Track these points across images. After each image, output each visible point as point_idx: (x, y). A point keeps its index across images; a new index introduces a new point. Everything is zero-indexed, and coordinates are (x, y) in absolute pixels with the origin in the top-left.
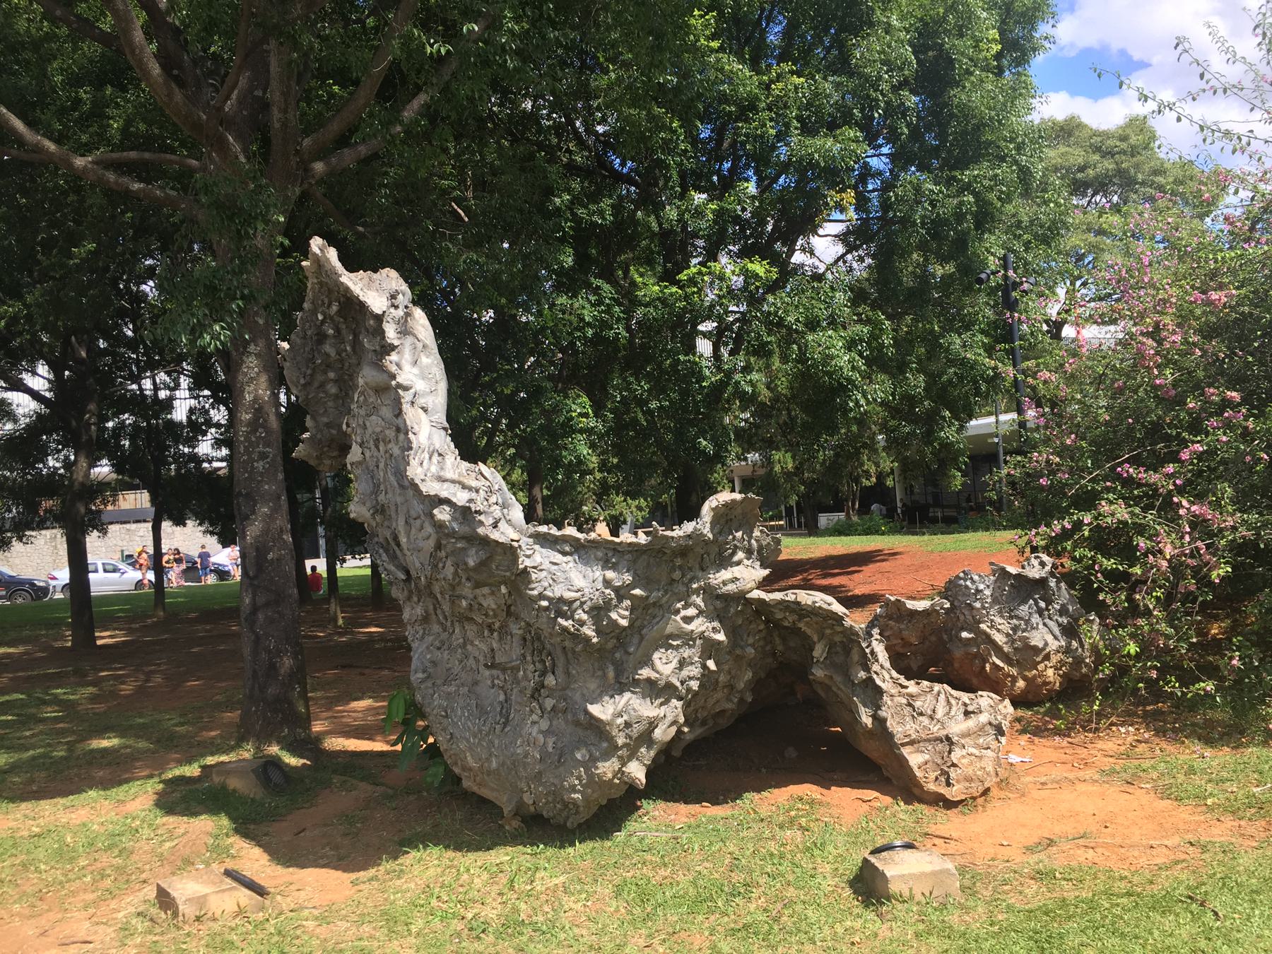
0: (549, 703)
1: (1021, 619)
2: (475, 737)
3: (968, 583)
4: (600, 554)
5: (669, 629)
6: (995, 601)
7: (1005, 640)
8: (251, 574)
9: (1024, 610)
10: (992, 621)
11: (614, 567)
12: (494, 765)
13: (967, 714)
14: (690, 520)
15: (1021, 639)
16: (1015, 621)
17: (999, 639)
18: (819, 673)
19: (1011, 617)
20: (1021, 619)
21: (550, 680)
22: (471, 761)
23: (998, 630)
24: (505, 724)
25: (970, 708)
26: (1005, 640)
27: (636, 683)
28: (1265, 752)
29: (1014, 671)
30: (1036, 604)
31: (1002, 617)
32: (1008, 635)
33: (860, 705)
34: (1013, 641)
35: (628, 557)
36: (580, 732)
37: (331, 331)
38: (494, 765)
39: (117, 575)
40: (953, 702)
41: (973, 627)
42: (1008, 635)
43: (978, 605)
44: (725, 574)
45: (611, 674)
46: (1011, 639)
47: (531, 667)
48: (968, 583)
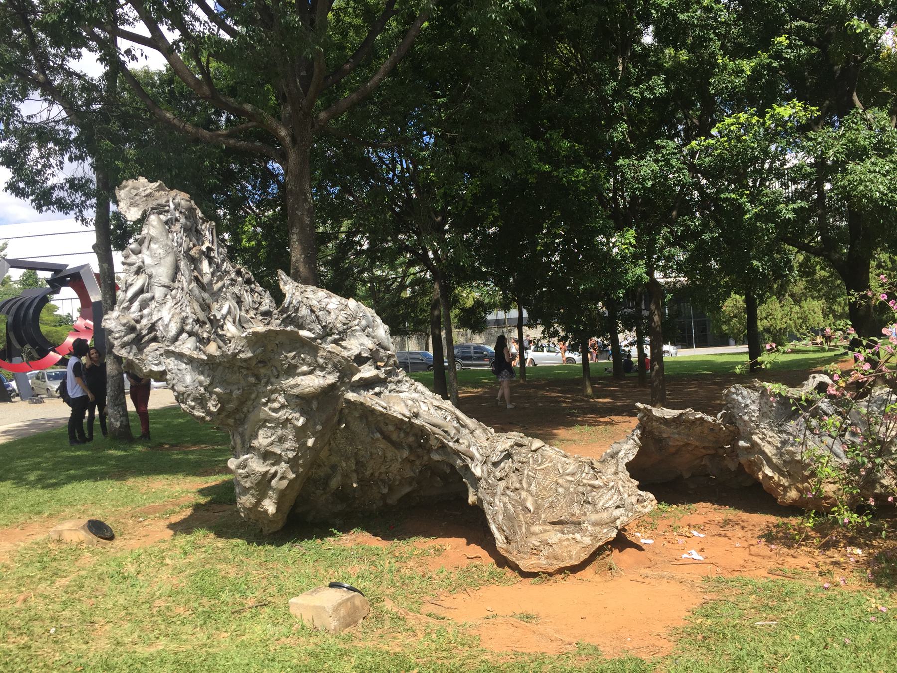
1: (788, 433)
3: (740, 398)
5: (262, 416)
6: (763, 415)
7: (775, 451)
9: (791, 426)
10: (763, 433)
11: (202, 373)
15: (789, 452)
16: (784, 436)
17: (769, 450)
19: (780, 432)
20: (788, 433)
23: (769, 443)
26: (775, 451)
27: (254, 448)
28: (877, 600)
29: (785, 481)
30: (807, 421)
31: (772, 430)
32: (777, 448)
33: (469, 485)
34: (782, 454)
39: (554, 354)
41: (749, 439)
42: (777, 448)
43: (746, 418)
44: (291, 381)
46: (780, 452)
48: (740, 398)
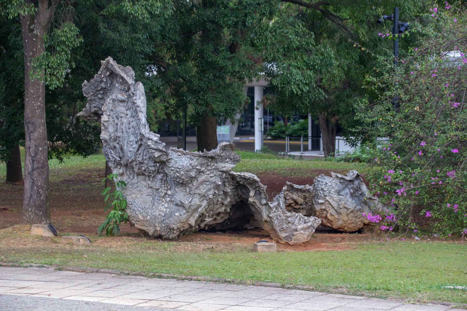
0: (168, 199)
2: (142, 209)
4: (189, 156)
8: (32, 155)
12: (149, 218)
13: (305, 223)
14: (214, 149)
18: (251, 200)
19: (339, 195)
21: (169, 192)
22: (140, 217)
24: (153, 206)
25: (307, 221)
35: (197, 158)
36: (177, 207)
37: (105, 80)
38: (149, 218)
40: (302, 219)
45: (188, 190)
47: (164, 188)
